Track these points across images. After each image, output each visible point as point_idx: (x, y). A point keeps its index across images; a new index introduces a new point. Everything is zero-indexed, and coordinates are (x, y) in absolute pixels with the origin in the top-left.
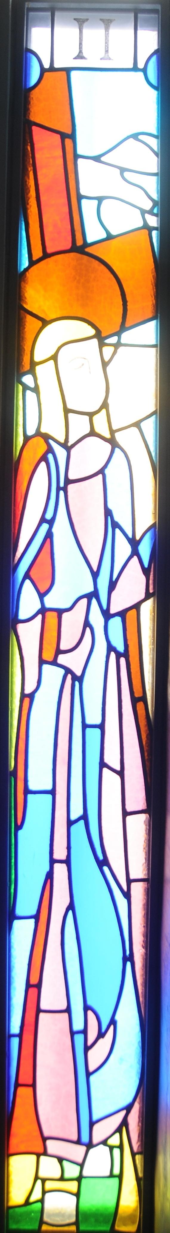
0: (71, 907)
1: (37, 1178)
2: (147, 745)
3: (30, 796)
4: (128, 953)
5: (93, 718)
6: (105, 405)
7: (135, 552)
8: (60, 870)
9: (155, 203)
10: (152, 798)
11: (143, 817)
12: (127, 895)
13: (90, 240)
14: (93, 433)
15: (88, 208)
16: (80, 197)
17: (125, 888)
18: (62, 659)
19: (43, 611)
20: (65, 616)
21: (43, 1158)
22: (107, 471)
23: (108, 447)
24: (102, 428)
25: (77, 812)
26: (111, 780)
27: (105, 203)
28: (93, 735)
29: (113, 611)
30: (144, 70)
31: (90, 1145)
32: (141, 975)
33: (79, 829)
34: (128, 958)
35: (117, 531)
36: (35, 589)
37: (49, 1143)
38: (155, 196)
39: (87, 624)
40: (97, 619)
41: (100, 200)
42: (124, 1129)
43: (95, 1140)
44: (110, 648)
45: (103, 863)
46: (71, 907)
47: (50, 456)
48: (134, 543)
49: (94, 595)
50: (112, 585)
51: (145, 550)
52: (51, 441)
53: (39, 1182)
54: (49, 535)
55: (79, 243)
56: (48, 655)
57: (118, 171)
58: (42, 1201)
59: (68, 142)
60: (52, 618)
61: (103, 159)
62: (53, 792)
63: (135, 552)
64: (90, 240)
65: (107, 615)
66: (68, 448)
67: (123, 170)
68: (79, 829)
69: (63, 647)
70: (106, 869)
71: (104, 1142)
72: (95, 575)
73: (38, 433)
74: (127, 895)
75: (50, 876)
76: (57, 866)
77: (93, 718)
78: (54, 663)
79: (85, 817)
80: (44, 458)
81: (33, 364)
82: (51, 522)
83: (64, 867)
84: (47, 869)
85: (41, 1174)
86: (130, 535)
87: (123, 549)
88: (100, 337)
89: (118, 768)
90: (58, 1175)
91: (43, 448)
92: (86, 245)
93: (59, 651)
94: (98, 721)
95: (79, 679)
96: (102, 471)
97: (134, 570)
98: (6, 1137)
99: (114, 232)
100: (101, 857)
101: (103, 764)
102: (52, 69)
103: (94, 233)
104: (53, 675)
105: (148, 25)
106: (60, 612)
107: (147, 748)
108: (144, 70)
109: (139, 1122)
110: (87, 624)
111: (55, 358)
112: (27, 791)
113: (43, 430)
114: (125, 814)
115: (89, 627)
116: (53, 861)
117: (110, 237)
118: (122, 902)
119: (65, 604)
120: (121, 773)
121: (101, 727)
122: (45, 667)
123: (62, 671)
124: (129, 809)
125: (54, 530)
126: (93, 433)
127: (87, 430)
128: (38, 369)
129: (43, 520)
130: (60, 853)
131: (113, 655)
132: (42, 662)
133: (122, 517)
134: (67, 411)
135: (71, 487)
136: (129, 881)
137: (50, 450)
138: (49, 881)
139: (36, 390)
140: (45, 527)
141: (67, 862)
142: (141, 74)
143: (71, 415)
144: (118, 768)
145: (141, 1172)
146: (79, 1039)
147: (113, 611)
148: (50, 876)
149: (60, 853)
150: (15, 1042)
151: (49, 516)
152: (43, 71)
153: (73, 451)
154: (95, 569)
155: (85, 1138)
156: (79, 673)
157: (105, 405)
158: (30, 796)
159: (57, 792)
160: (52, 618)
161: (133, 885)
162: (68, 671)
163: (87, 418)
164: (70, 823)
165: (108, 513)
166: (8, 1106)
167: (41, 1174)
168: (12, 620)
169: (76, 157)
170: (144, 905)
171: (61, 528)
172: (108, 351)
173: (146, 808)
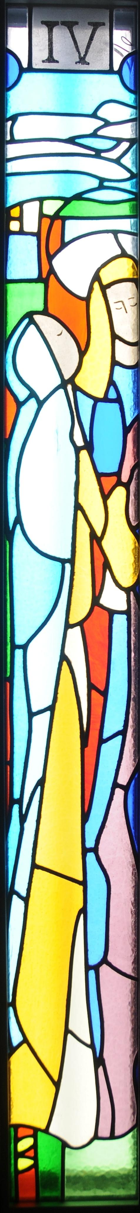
2: (134, 519)
9: (133, 176)
10: (135, 839)
11: (11, 274)
30: (119, 73)
32: (131, 1046)
36: (18, 323)
38: (130, 41)
98: (5, 837)
105: (123, 24)
107: (134, 638)
108: (119, 73)
109: (134, 447)
142: (116, 77)
145: (132, 517)
152: (22, 70)
159: (97, 741)
168: (5, 341)
170: (132, 1029)
173: (93, 27)
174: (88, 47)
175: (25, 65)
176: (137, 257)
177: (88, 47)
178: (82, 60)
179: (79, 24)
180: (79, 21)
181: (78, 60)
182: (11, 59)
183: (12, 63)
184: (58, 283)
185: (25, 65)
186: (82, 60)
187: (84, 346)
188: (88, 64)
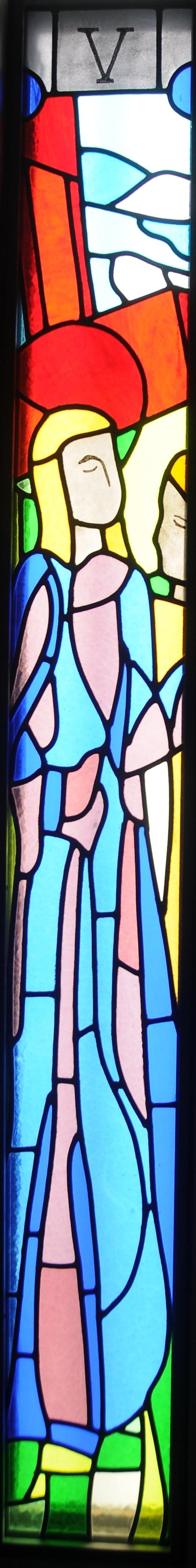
0: (79, 1137)
1: (38, 1471)
3: (28, 1000)
5: (106, 904)
6: (120, 518)
7: (156, 699)
8: (65, 1092)
13: (101, 308)
14: (105, 551)
15: (99, 268)
17: (145, 1114)
18: (68, 829)
19: (45, 769)
20: (71, 775)
21: (48, 1448)
22: (123, 596)
23: (125, 568)
24: (116, 544)
25: (85, 1021)
26: (128, 982)
27: (119, 260)
28: (106, 926)
29: (128, 768)
30: (169, 91)
31: (103, 1433)
33: (87, 1042)
34: (149, 1207)
35: (134, 671)
37: (54, 1428)
39: (98, 787)
40: (109, 779)
41: (112, 257)
42: (146, 1414)
44: (128, 816)
45: (118, 1085)
46: (79, 1137)
47: (51, 579)
48: (155, 686)
50: (128, 739)
51: (168, 694)
52: (53, 561)
53: (42, 1478)
54: (51, 679)
55: (88, 314)
56: (51, 824)
58: (47, 1497)
59: (74, 185)
60: (54, 778)
63: (156, 699)
64: (101, 308)
65: (122, 775)
66: (74, 568)
67: (141, 219)
68: (87, 1042)
69: (69, 813)
70: (121, 1092)
72: (108, 724)
73: (38, 549)
74: (148, 1123)
75: (52, 1100)
76: (60, 1086)
77: (106, 904)
78: (58, 833)
79: (94, 1027)
80: (44, 581)
82: (53, 661)
83: (30, 1362)
84: (49, 1089)
86: (150, 676)
87: (141, 692)
88: (115, 431)
91: (44, 567)
92: (96, 314)
93: (64, 819)
95: (88, 855)
96: (116, 597)
97: (154, 719)
99: (130, 298)
100: (116, 1078)
101: (117, 963)
102: (55, 92)
103: (105, 300)
104: (56, 848)
106: (65, 772)
108: (169, 91)
110: (98, 787)
111: (58, 456)
112: (25, 994)
114: (146, 1022)
115: (101, 792)
116: (56, 1080)
117: (126, 303)
120: (140, 973)
121: (116, 915)
122: (48, 839)
124: (150, 1016)
126: (105, 551)
128: (37, 469)
129: (43, 658)
130: (66, 1070)
131: (130, 825)
132: (43, 833)
133: (140, 654)
134: (73, 523)
135: (76, 616)
136: (150, 1106)
137: (51, 571)
138: (51, 1108)
139: (34, 496)
141: (75, 1081)
142: (165, 97)
147: (128, 768)
148: (52, 1100)
149: (66, 1070)
151: (50, 653)
152: (45, 95)
153: (80, 575)
154: (108, 717)
155: (97, 1424)
156: (88, 847)
157: (120, 518)
160: (54, 778)
161: (155, 1111)
162: (74, 844)
163: (97, 532)
164: (77, 1035)
165: (124, 651)
167: (45, 1466)
169: (83, 204)
172: (125, 440)
174: (112, 62)
175: (49, 89)
176: (32, 81)
177: (112, 62)
178: (106, 78)
179: (135, 29)
180: (132, 27)
181: (101, 77)
182: (33, 82)
183: (34, 88)
184: (161, 547)
185: (49, 89)
186: (106, 78)
187: (35, 108)
188: (112, 81)
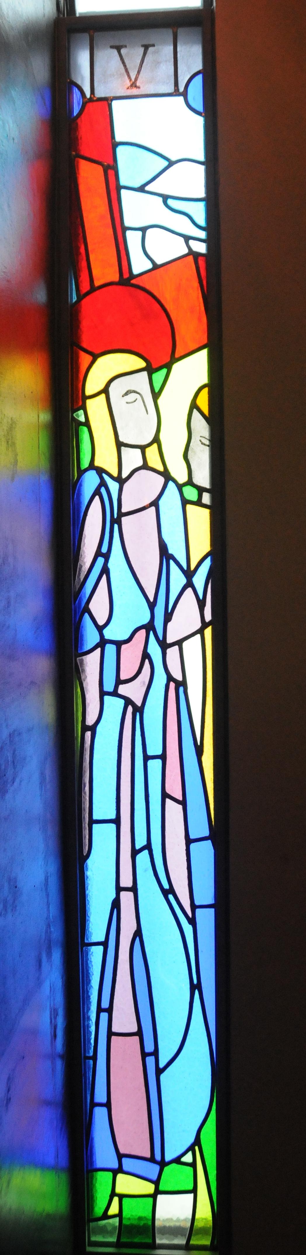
0: (138, 933)
4: (195, 981)
5: (154, 748)
6: (156, 440)
7: (190, 584)
8: (127, 898)
12: (192, 921)
14: (145, 466)
15: (133, 239)
16: (125, 229)
17: (190, 914)
18: (122, 689)
19: (103, 643)
21: (120, 1176)
22: (161, 503)
25: (141, 842)
26: (174, 810)
27: (149, 232)
28: (155, 766)
29: (169, 640)
30: (185, 94)
33: (143, 858)
34: (196, 987)
35: (172, 562)
37: (124, 1160)
39: (146, 656)
40: (154, 649)
41: (144, 230)
42: (197, 1148)
43: (168, 1158)
44: (170, 678)
46: (138, 933)
47: (103, 490)
48: (189, 574)
49: (149, 627)
50: (168, 617)
51: (199, 580)
53: (116, 1200)
54: (105, 571)
55: (126, 276)
56: (109, 686)
57: (161, 199)
60: (110, 650)
61: (147, 188)
62: (117, 822)
63: (190, 584)
65: (164, 646)
66: (121, 481)
67: (165, 198)
68: (143, 858)
69: (123, 677)
70: (171, 897)
71: (177, 1160)
72: (152, 606)
74: (192, 921)
75: (116, 904)
78: (115, 693)
79: (148, 846)
80: (97, 492)
81: (85, 398)
82: (107, 556)
84: (114, 896)
85: (118, 1190)
87: (178, 579)
88: (150, 370)
89: (180, 798)
90: (113, 826)
91: (97, 481)
92: (132, 276)
93: (119, 682)
94: (160, 752)
95: (139, 710)
96: (155, 504)
97: (189, 599)
100: (166, 886)
101: (165, 795)
103: (139, 265)
104: (114, 705)
106: (119, 644)
108: (185, 94)
110: (146, 656)
111: (105, 391)
112: (92, 822)
113: (97, 463)
114: (189, 841)
116: (119, 889)
117: (156, 267)
118: (188, 929)
119: (124, 636)
120: (183, 803)
121: (163, 757)
122: (107, 698)
123: (122, 702)
125: (110, 565)
126: (145, 466)
127: (140, 463)
129: (98, 553)
130: (126, 881)
131: (172, 685)
132: (103, 694)
133: (176, 549)
134: (120, 445)
136: (194, 907)
137: (103, 483)
139: (87, 424)
140: (101, 561)
141: (134, 889)
143: (123, 449)
144: (180, 798)
146: (150, 1060)
147: (169, 640)
148: (116, 904)
149: (126, 881)
150: (96, 953)
151: (104, 549)
153: (126, 486)
154: (151, 599)
155: (158, 1157)
156: (139, 703)
157: (156, 440)
158: (95, 826)
160: (110, 650)
161: (198, 911)
162: (128, 702)
163: (138, 451)
164: (135, 853)
166: (86, 1111)
167: (118, 1190)
171: (116, 562)
